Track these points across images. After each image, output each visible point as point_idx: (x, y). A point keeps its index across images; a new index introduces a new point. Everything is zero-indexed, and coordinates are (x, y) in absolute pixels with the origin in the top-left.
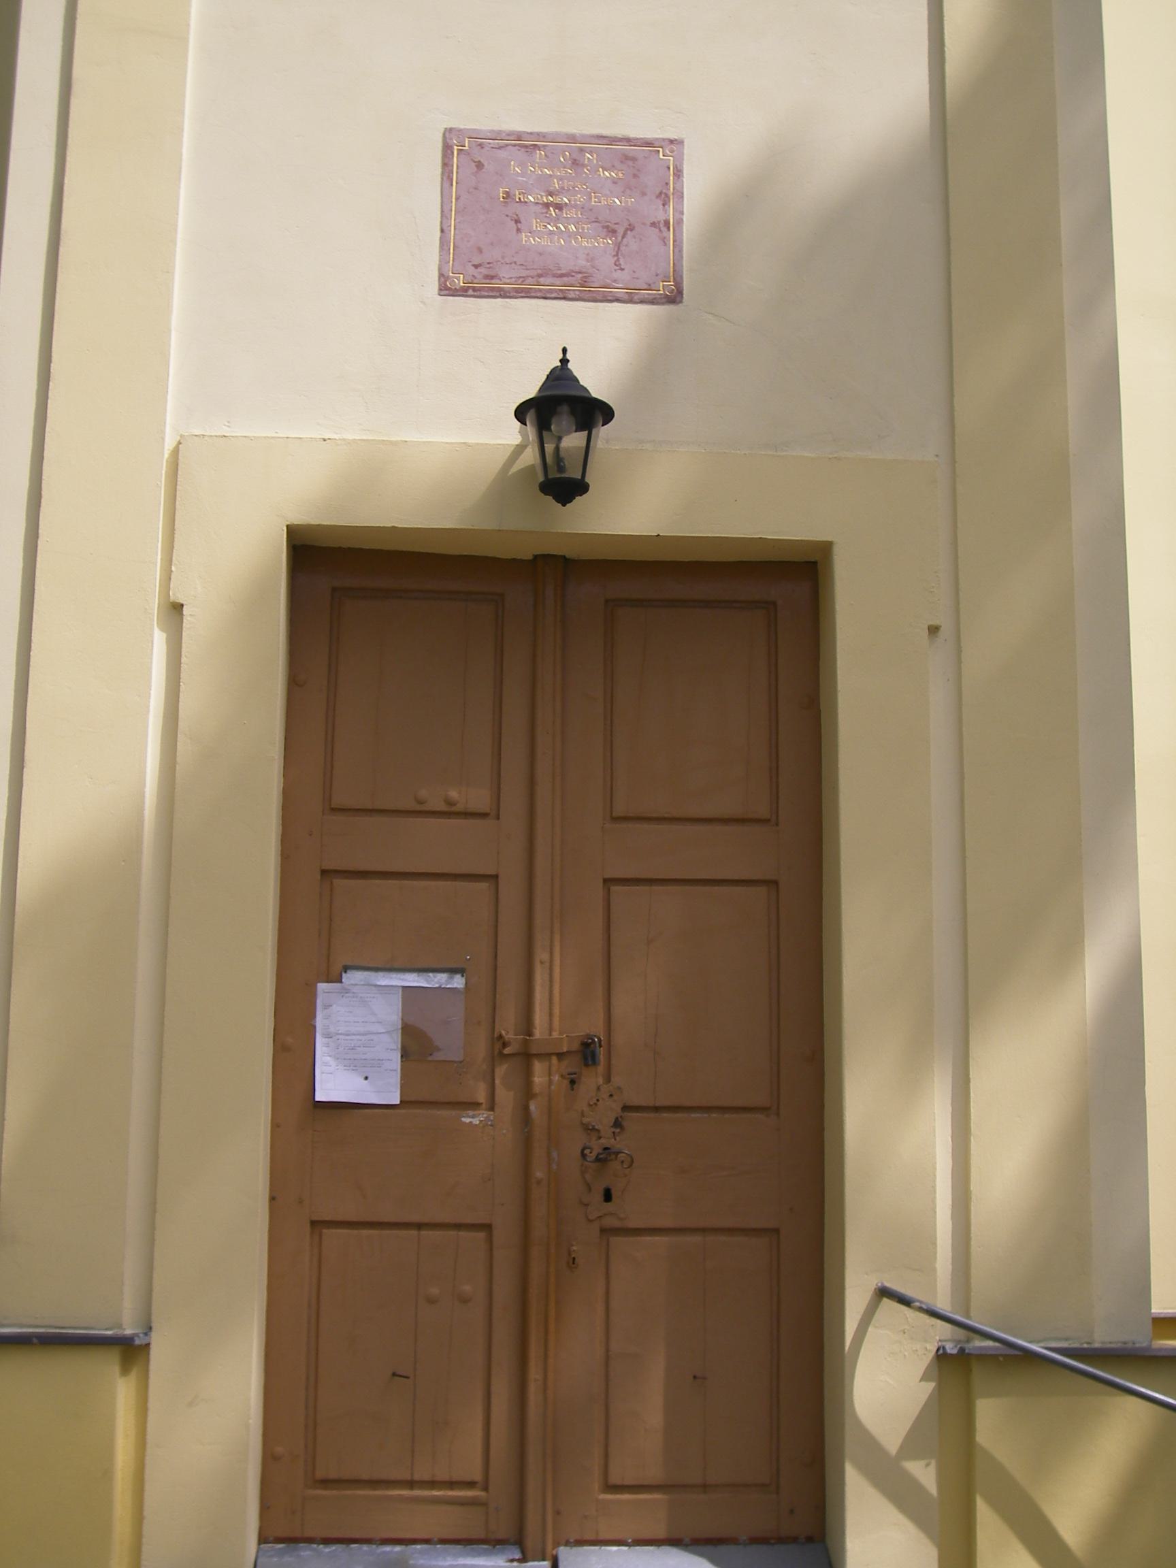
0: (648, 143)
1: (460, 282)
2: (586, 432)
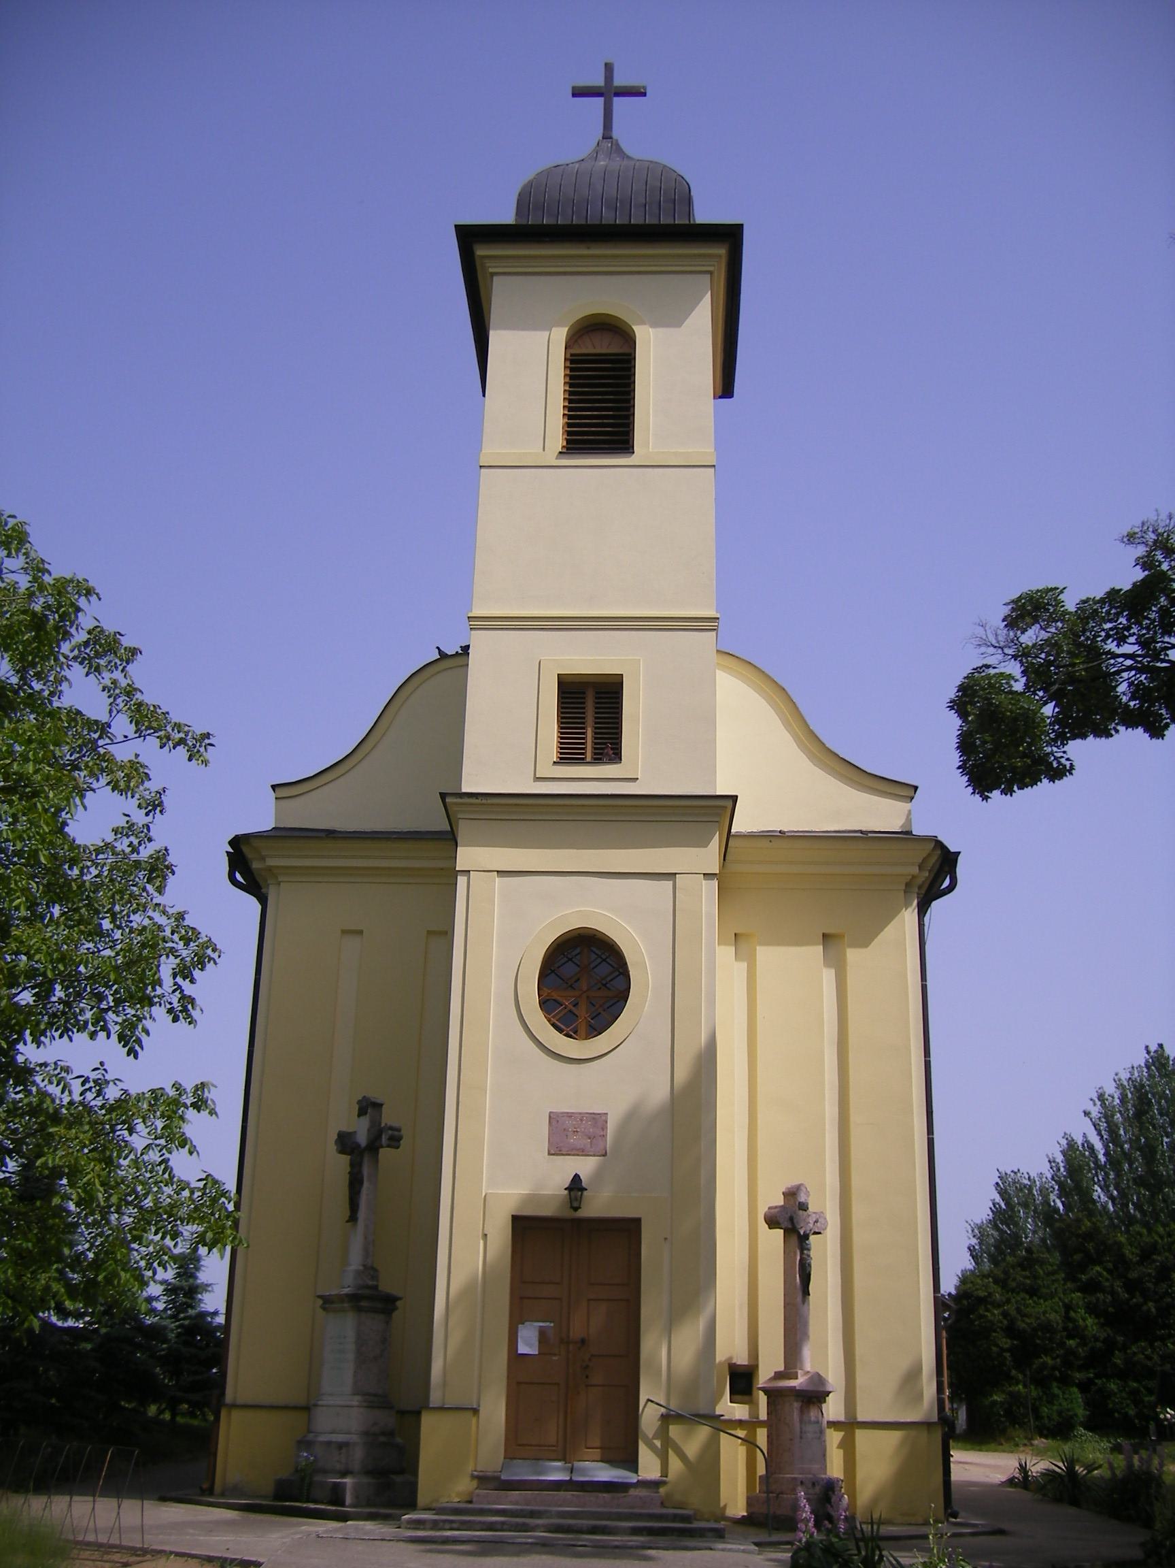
0: (599, 1114)
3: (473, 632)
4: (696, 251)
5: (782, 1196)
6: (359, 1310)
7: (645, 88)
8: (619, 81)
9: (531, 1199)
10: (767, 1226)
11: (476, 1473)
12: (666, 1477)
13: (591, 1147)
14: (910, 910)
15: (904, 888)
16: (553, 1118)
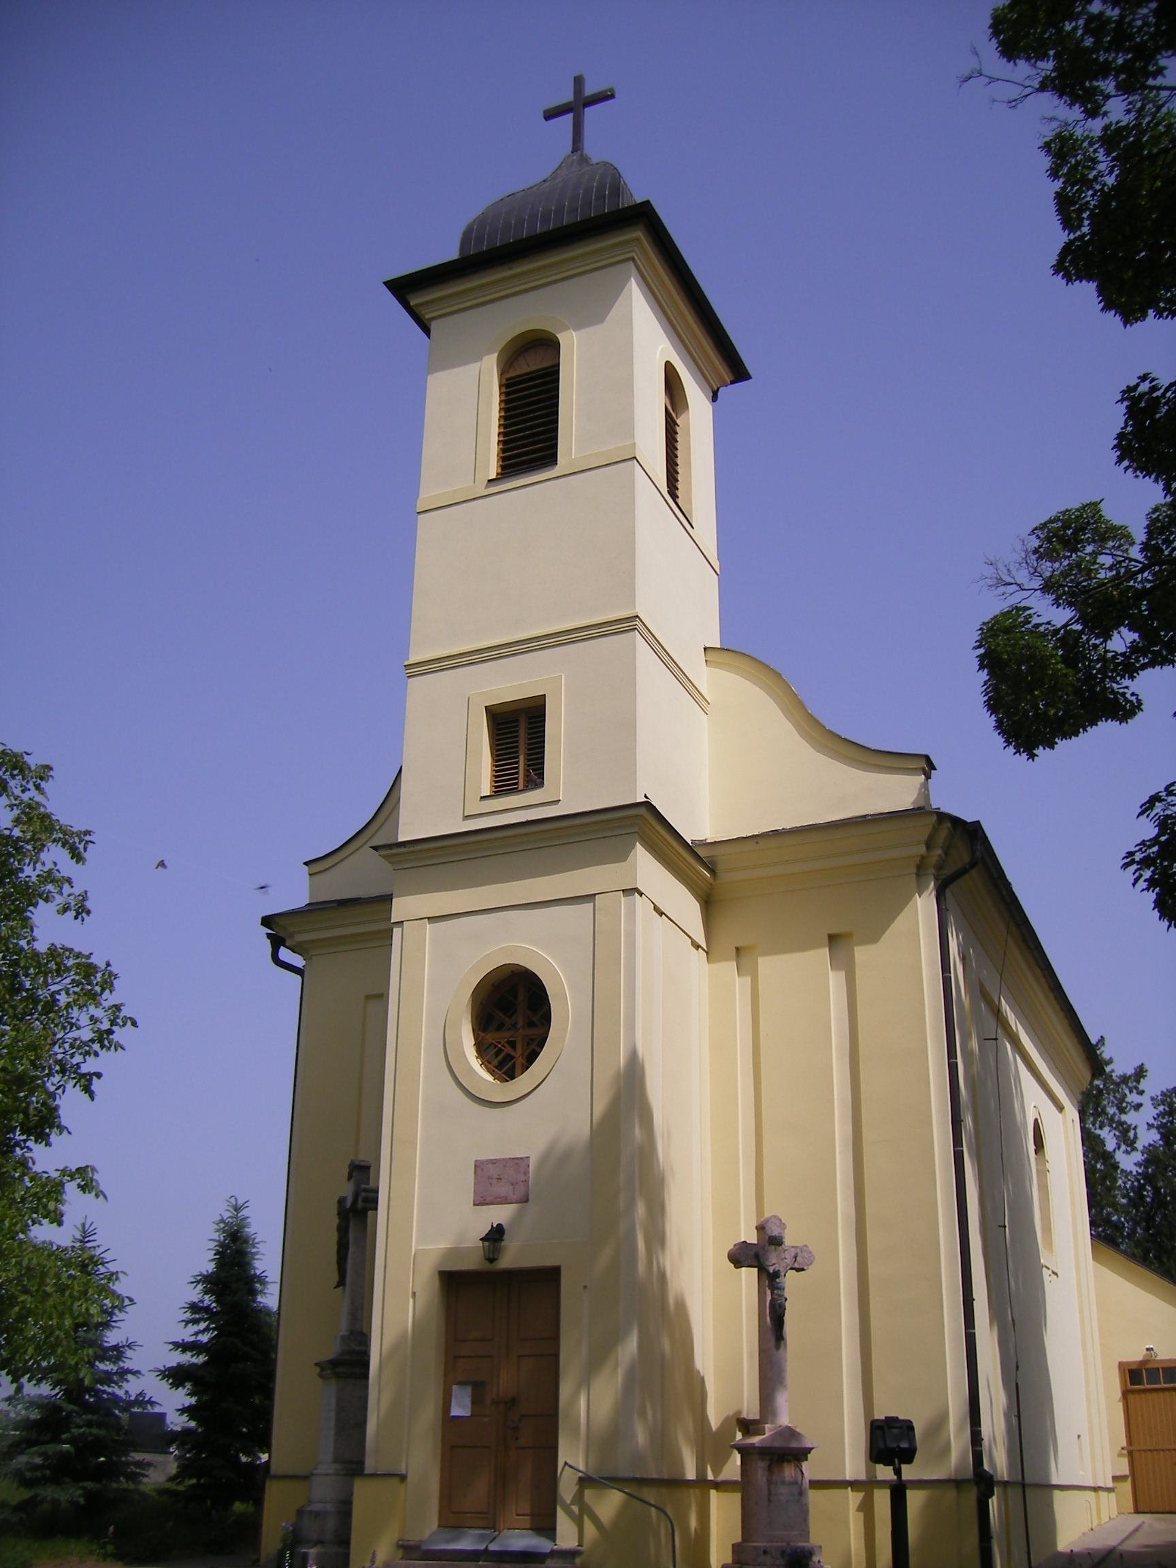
0: (521, 1158)
1: (478, 1202)
2: (592, 904)
3: (410, 680)
4: (599, 245)
5: (756, 1231)
6: (338, 1376)
7: (611, 90)
8: (590, 90)
9: (452, 1253)
10: (732, 1265)
11: (401, 1542)
12: (582, 1546)
13: (514, 1194)
14: (925, 894)
15: (914, 870)
16: (479, 1166)
